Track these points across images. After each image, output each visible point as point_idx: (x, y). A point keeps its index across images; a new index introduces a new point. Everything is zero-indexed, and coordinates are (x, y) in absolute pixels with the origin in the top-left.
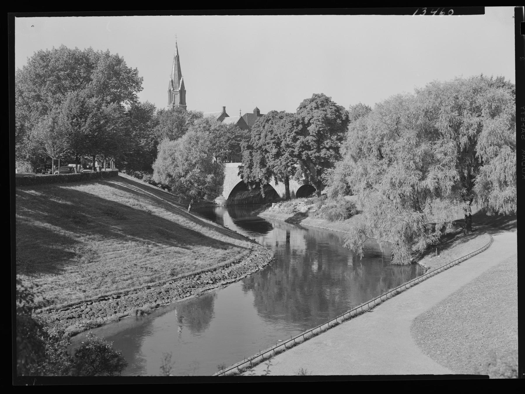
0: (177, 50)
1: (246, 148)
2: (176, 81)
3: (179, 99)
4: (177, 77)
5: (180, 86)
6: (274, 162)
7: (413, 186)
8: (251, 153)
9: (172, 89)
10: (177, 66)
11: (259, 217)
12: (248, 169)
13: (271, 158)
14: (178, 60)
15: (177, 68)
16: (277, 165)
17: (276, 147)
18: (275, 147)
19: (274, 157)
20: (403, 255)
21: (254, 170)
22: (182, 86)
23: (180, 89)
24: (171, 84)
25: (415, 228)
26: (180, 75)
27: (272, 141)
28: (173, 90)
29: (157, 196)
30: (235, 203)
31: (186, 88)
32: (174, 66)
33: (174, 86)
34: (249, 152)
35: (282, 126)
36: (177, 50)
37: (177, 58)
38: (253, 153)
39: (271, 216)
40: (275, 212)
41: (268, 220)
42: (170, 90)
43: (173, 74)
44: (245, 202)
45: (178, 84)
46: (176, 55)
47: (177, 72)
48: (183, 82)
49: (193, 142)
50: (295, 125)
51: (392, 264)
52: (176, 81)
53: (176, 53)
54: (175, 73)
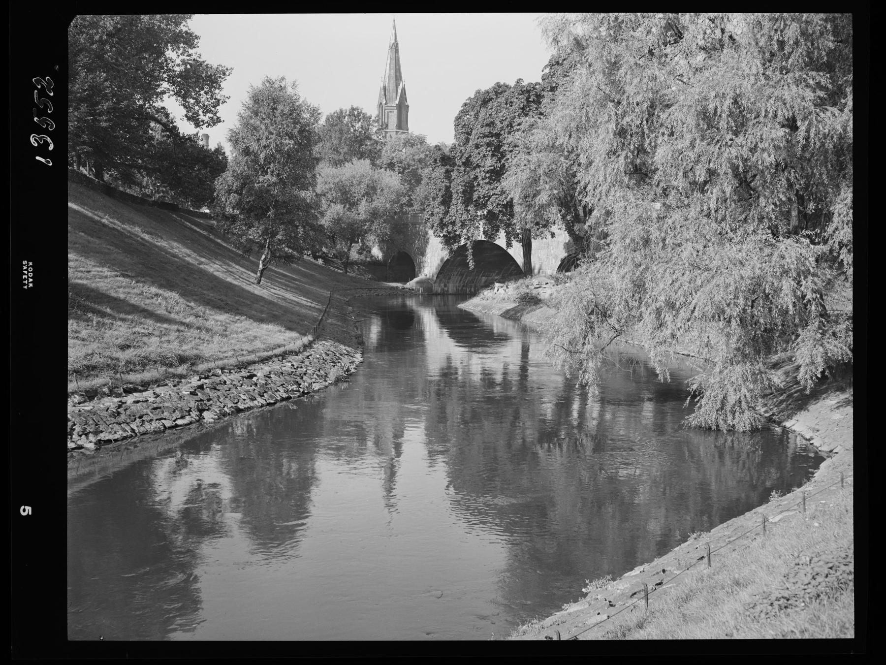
0: (395, 33)
1: (439, 164)
2: (391, 88)
3: (396, 119)
4: (393, 81)
5: (398, 97)
6: (488, 187)
7: (791, 124)
8: (447, 171)
9: (384, 102)
10: (393, 62)
11: (461, 310)
12: (442, 207)
13: (483, 179)
14: (397, 51)
15: (393, 66)
16: (494, 194)
17: (493, 155)
18: (490, 153)
19: (490, 178)
20: (732, 399)
21: (453, 210)
22: (401, 96)
23: (397, 102)
24: (383, 93)
25: (787, 300)
26: (398, 77)
27: (485, 139)
28: (386, 104)
29: (93, 208)
30: (450, 291)
31: (410, 102)
32: (389, 62)
33: (388, 97)
34: (443, 170)
35: (506, 104)
36: (395, 33)
37: (395, 48)
38: (454, 174)
39: (484, 307)
40: (495, 301)
41: (477, 314)
42: (381, 103)
43: (387, 75)
44: (470, 291)
45: (395, 94)
46: (393, 41)
47: (393, 72)
48: (404, 90)
49: (264, 109)
50: (533, 101)
51: (690, 428)
52: (391, 88)
53: (394, 38)
54: (390, 74)
